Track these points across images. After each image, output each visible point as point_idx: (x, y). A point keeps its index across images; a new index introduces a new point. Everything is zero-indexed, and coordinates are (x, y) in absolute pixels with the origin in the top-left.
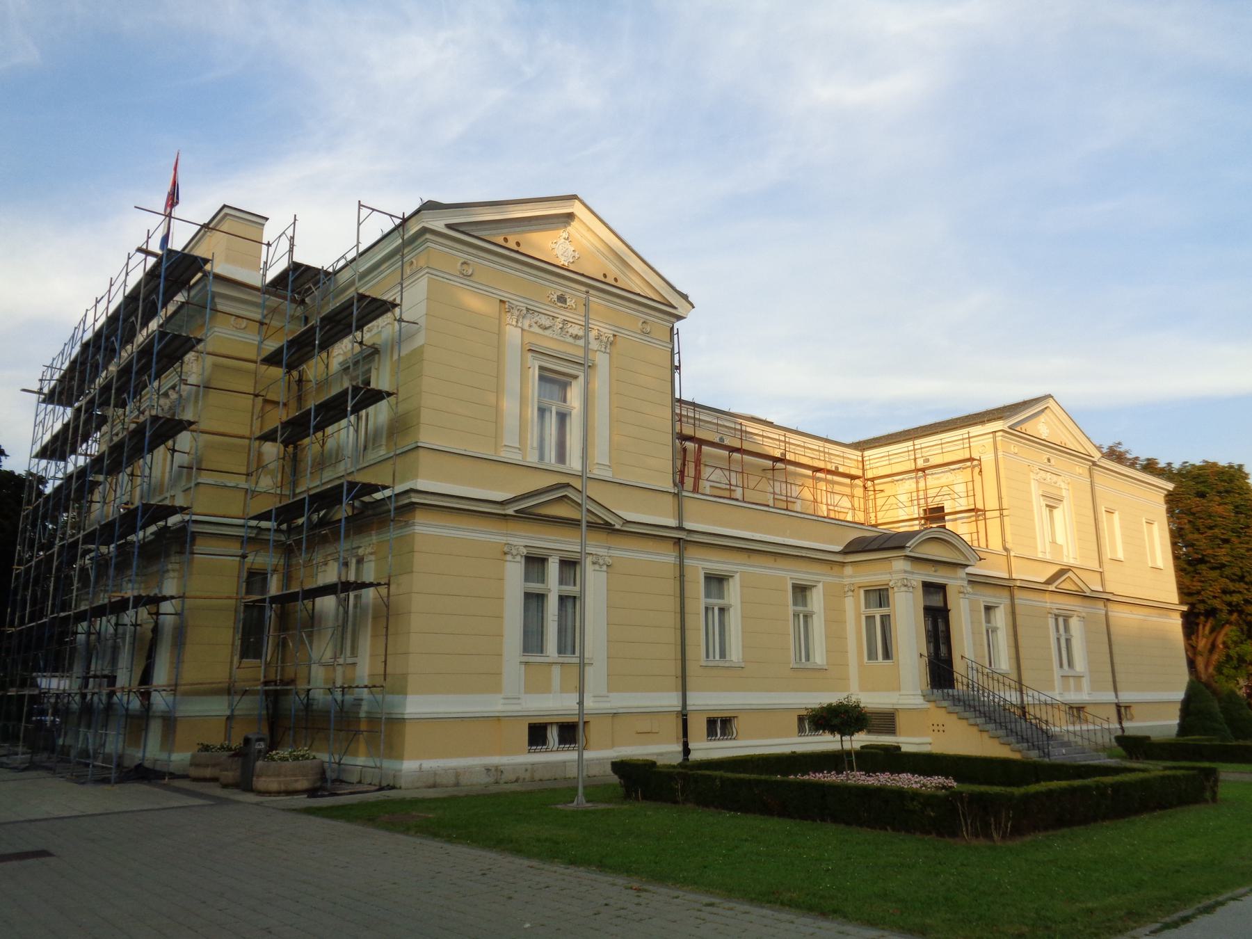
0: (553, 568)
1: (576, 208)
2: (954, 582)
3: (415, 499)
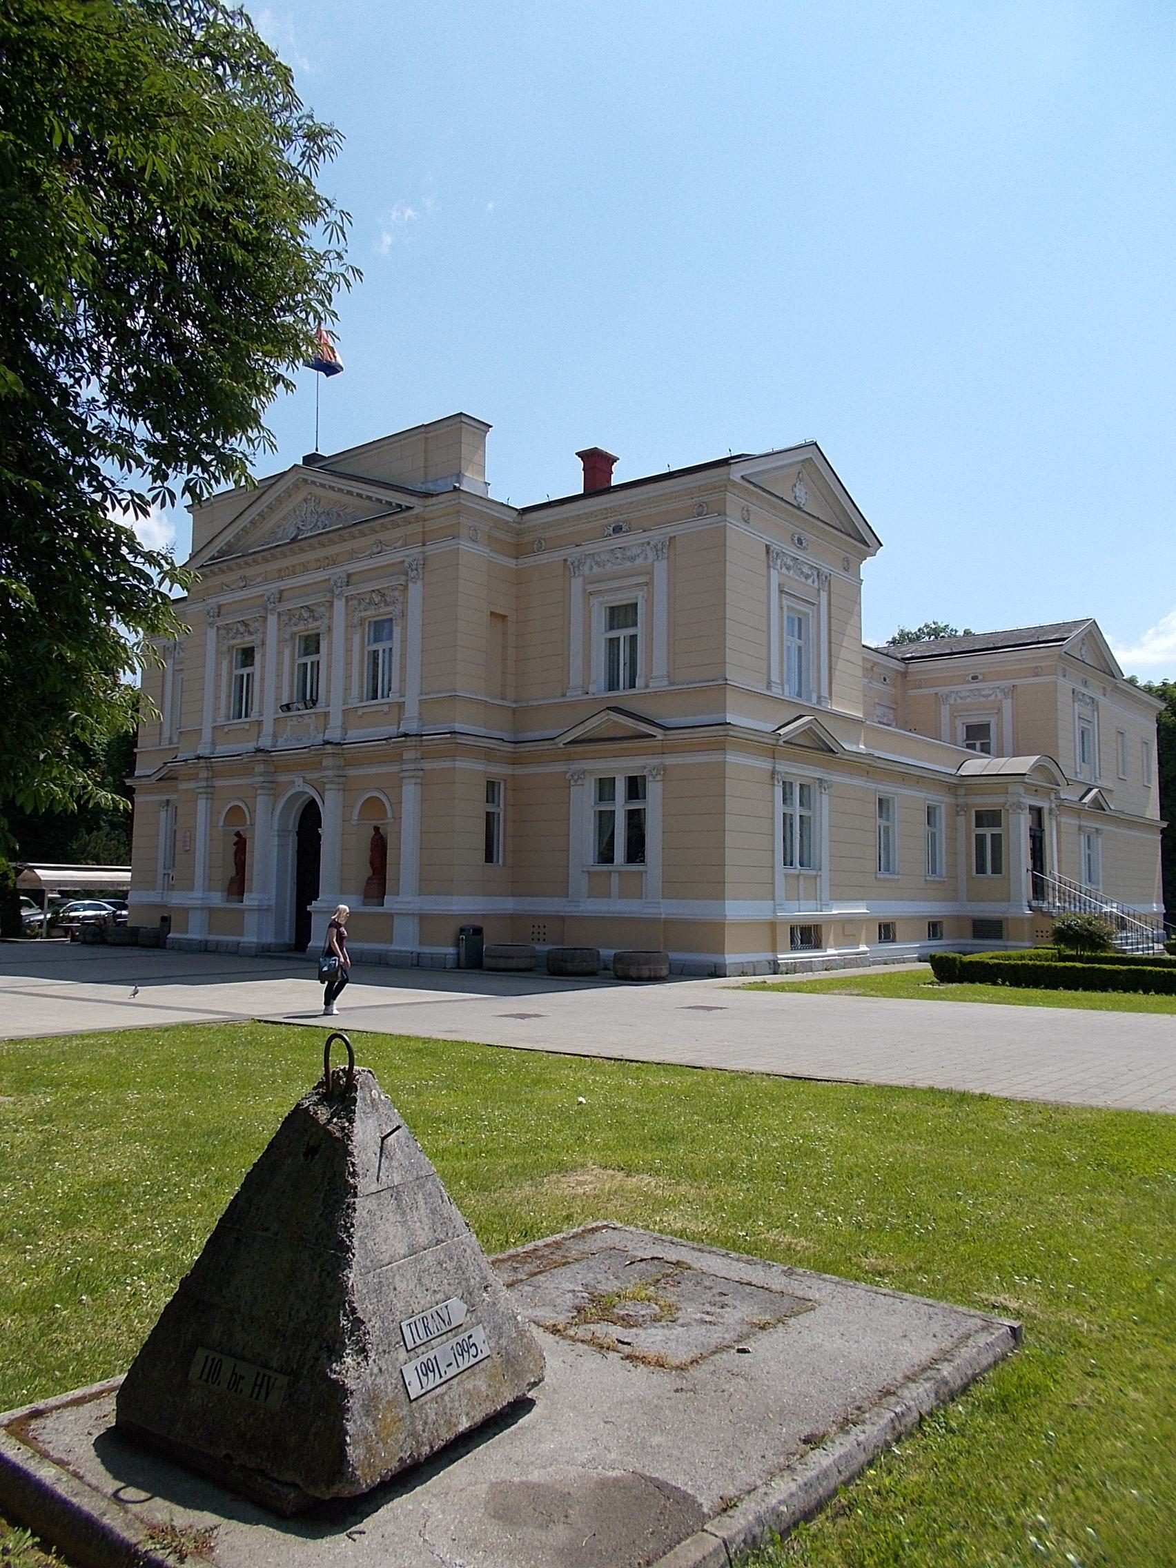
0: (621, 789)
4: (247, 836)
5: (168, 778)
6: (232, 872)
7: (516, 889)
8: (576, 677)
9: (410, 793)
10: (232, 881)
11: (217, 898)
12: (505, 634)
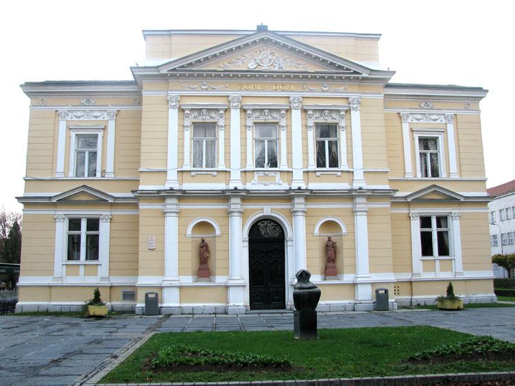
9: (361, 221)
11: (188, 280)
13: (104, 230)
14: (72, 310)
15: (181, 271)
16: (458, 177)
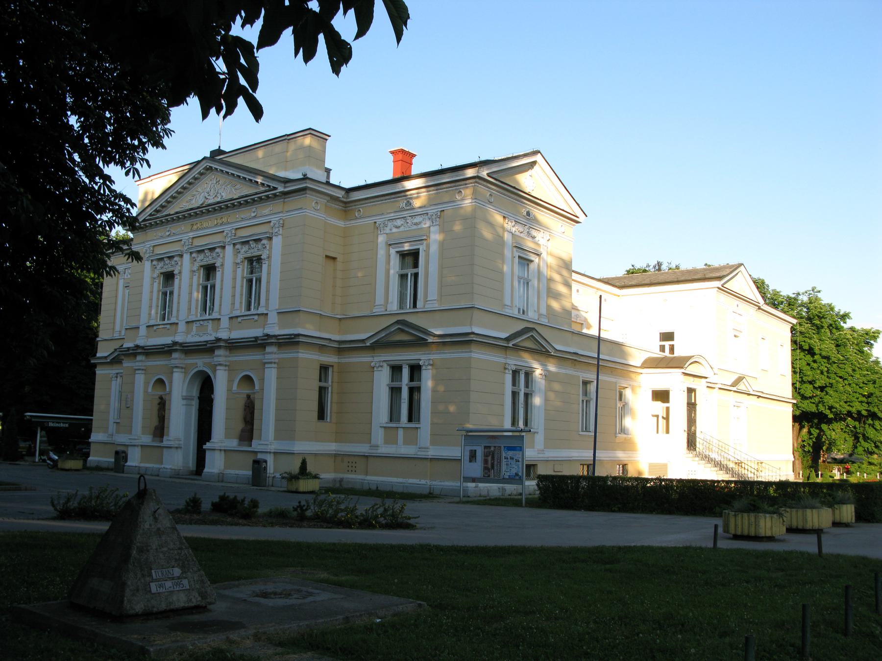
0: (406, 372)
1: (538, 158)
2: (699, 386)
3: (301, 339)
4: (166, 397)
5: (116, 360)
6: (155, 422)
7: (339, 437)
8: (380, 299)
10: (156, 428)
12: (335, 270)
13: (428, 382)
14: (395, 489)
15: (227, 436)
16: (437, 305)
